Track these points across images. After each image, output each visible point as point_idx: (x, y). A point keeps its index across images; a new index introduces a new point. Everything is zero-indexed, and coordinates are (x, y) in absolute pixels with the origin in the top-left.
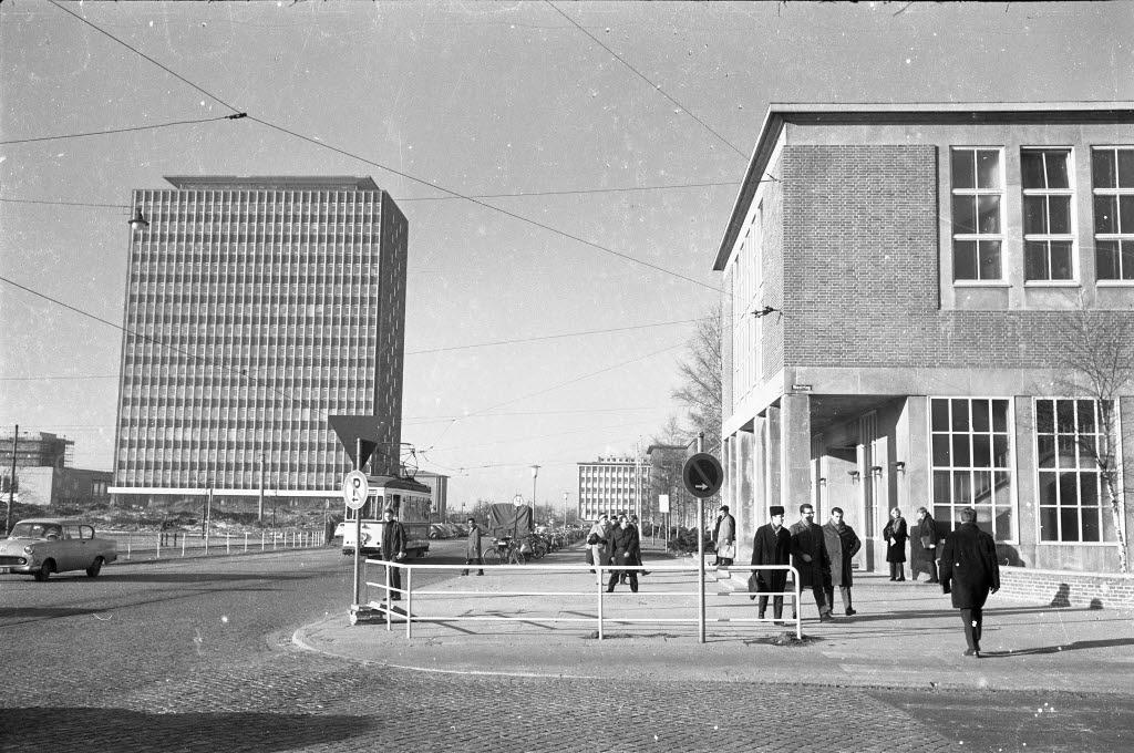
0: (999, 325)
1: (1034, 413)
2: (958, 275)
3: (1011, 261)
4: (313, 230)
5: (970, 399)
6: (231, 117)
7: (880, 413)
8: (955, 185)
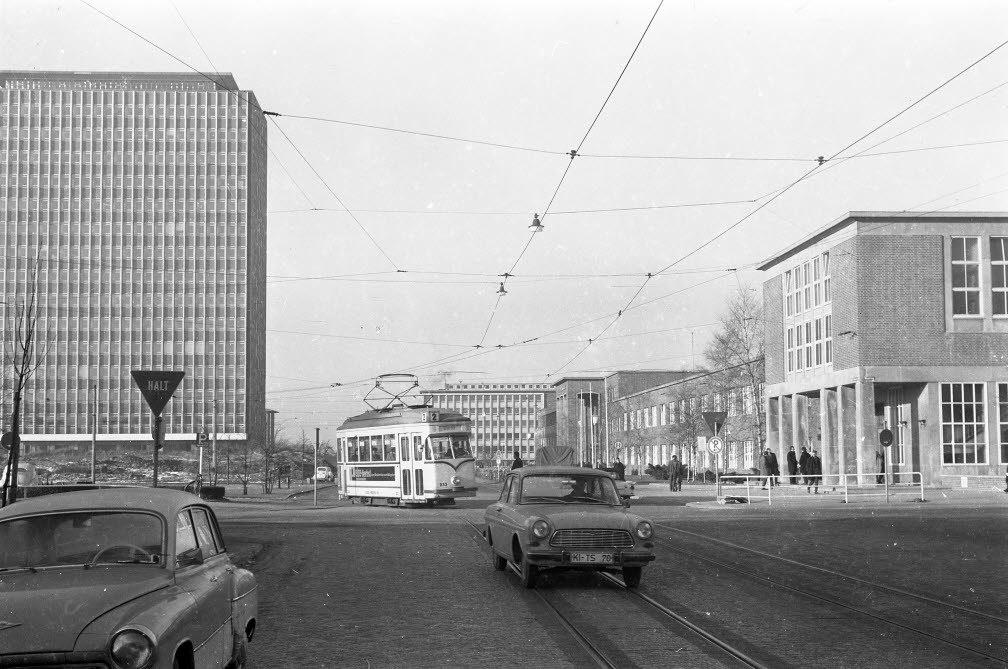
0: (979, 343)
1: (997, 390)
2: (955, 311)
3: (984, 303)
4: (169, 137)
5: (954, 464)
6: (277, 114)
7: (908, 391)
8: (954, 285)
